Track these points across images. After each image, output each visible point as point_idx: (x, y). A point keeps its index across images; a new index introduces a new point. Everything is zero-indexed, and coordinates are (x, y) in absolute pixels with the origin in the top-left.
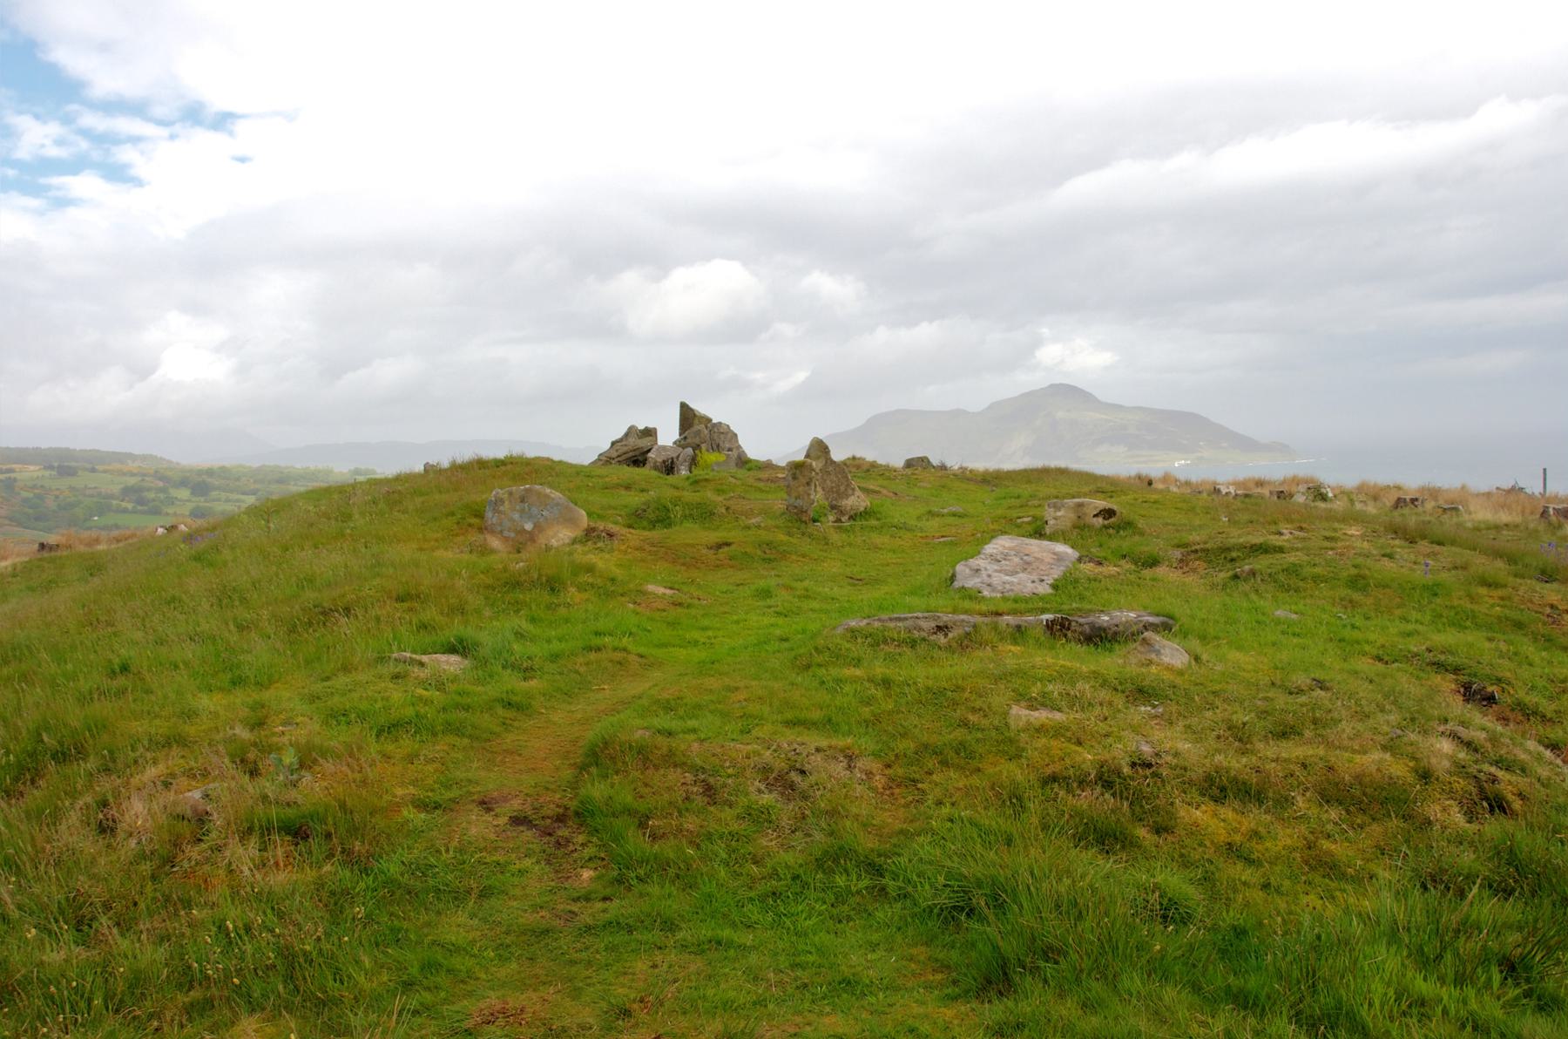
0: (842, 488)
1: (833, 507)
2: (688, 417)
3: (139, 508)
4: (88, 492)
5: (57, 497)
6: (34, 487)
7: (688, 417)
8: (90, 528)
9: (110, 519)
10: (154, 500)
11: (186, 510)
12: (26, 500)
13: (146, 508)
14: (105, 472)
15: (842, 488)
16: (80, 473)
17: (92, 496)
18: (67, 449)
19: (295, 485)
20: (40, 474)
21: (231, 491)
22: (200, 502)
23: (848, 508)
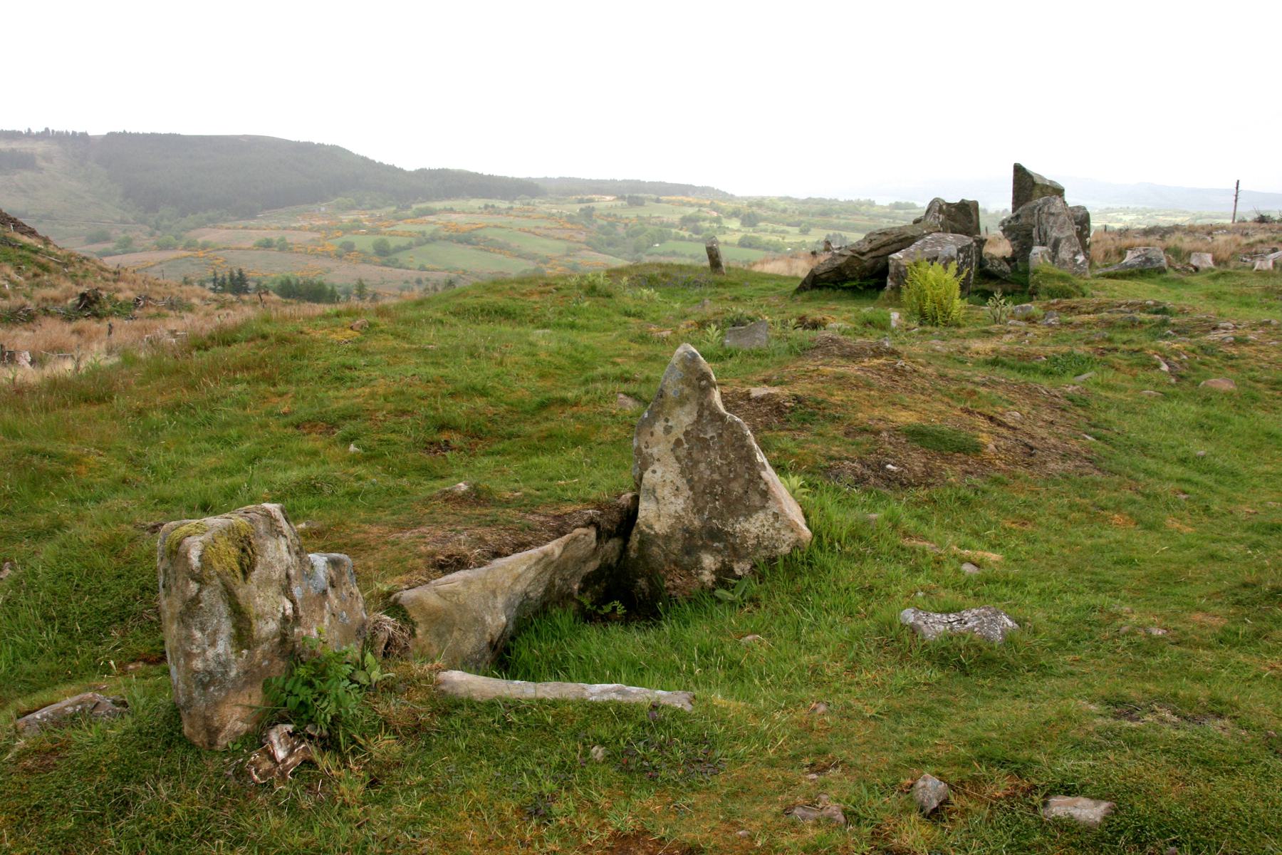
0: (737, 488)
1: (715, 535)
2: (1024, 183)
3: (695, 236)
4: (653, 220)
5: (626, 225)
6: (609, 215)
7: (1024, 183)
8: (651, 255)
9: (670, 245)
10: (708, 230)
11: (736, 238)
12: (601, 227)
13: (700, 237)
14: (668, 202)
15: (737, 488)
16: (646, 203)
17: (655, 224)
18: (638, 182)
19: (838, 217)
20: (613, 204)
21: (777, 222)
22: (750, 232)
23: (751, 542)
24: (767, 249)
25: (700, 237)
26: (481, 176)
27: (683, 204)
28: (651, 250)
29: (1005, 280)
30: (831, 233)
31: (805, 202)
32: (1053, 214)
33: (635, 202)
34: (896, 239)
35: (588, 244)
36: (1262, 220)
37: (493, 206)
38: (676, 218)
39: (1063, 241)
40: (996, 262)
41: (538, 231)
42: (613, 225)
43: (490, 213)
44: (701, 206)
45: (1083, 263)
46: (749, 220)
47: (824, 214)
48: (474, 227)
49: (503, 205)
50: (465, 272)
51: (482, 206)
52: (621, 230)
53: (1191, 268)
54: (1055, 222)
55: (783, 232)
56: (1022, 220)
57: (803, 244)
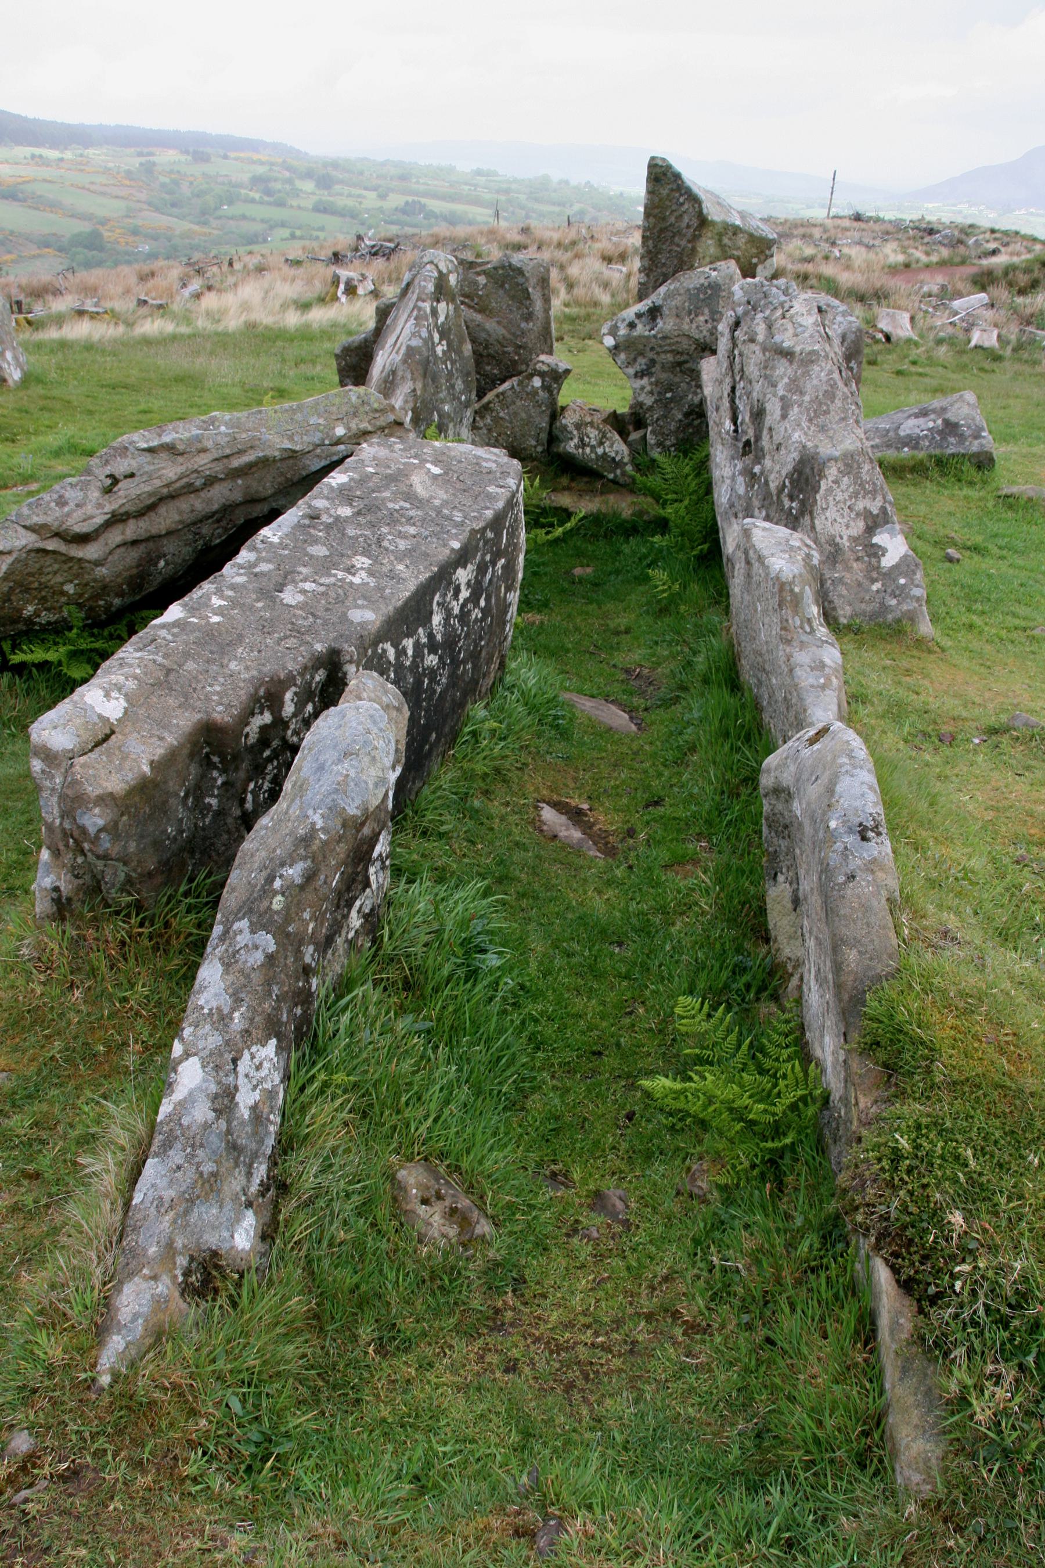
3: (266, 198)
4: (220, 180)
5: (191, 183)
6: (171, 172)
10: (280, 191)
11: (309, 203)
12: (163, 185)
14: (236, 159)
17: (223, 184)
22: (324, 196)
24: (343, 215)
25: (272, 199)
26: (25, 119)
27: (253, 162)
28: (219, 213)
29: (614, 482)
30: (410, 199)
31: (384, 164)
32: (788, 354)
33: (201, 157)
34: (218, 468)
35: (150, 204)
36: (858, 218)
37: (41, 156)
38: (245, 177)
39: (832, 472)
40: (593, 433)
41: (93, 188)
42: (176, 183)
43: (37, 165)
44: (272, 164)
45: (903, 567)
46: (325, 182)
47: (403, 178)
48: (20, 180)
49: (53, 154)
50: (12, 233)
51: (28, 156)
52: (185, 190)
53: (880, 336)
54: (795, 386)
55: (359, 196)
56: (666, 324)
57: (381, 210)
